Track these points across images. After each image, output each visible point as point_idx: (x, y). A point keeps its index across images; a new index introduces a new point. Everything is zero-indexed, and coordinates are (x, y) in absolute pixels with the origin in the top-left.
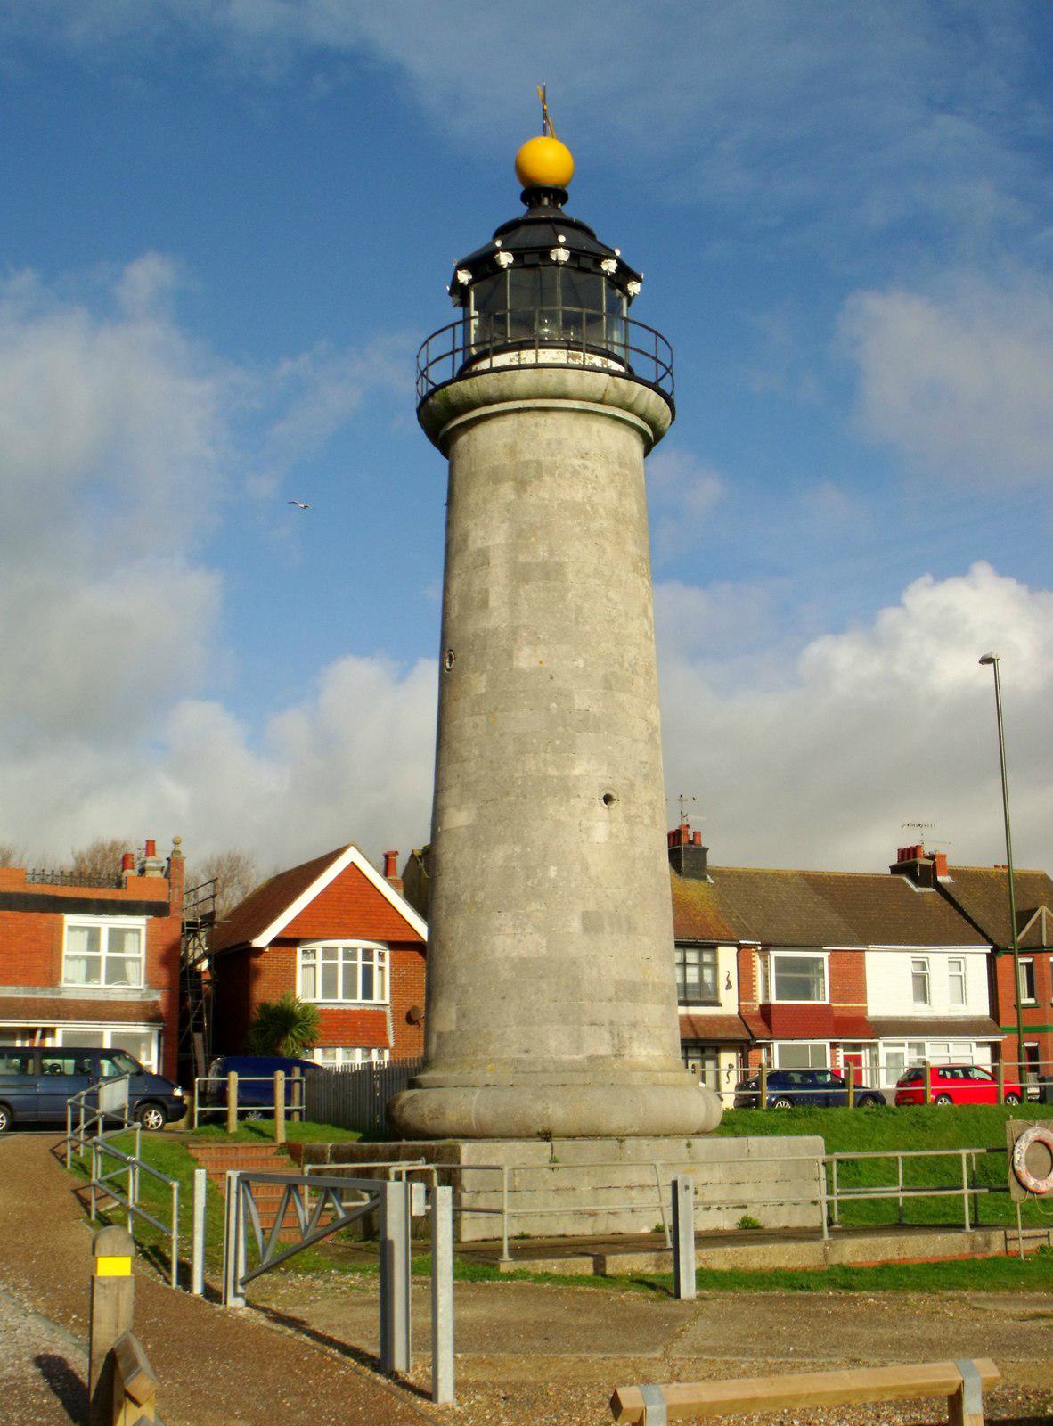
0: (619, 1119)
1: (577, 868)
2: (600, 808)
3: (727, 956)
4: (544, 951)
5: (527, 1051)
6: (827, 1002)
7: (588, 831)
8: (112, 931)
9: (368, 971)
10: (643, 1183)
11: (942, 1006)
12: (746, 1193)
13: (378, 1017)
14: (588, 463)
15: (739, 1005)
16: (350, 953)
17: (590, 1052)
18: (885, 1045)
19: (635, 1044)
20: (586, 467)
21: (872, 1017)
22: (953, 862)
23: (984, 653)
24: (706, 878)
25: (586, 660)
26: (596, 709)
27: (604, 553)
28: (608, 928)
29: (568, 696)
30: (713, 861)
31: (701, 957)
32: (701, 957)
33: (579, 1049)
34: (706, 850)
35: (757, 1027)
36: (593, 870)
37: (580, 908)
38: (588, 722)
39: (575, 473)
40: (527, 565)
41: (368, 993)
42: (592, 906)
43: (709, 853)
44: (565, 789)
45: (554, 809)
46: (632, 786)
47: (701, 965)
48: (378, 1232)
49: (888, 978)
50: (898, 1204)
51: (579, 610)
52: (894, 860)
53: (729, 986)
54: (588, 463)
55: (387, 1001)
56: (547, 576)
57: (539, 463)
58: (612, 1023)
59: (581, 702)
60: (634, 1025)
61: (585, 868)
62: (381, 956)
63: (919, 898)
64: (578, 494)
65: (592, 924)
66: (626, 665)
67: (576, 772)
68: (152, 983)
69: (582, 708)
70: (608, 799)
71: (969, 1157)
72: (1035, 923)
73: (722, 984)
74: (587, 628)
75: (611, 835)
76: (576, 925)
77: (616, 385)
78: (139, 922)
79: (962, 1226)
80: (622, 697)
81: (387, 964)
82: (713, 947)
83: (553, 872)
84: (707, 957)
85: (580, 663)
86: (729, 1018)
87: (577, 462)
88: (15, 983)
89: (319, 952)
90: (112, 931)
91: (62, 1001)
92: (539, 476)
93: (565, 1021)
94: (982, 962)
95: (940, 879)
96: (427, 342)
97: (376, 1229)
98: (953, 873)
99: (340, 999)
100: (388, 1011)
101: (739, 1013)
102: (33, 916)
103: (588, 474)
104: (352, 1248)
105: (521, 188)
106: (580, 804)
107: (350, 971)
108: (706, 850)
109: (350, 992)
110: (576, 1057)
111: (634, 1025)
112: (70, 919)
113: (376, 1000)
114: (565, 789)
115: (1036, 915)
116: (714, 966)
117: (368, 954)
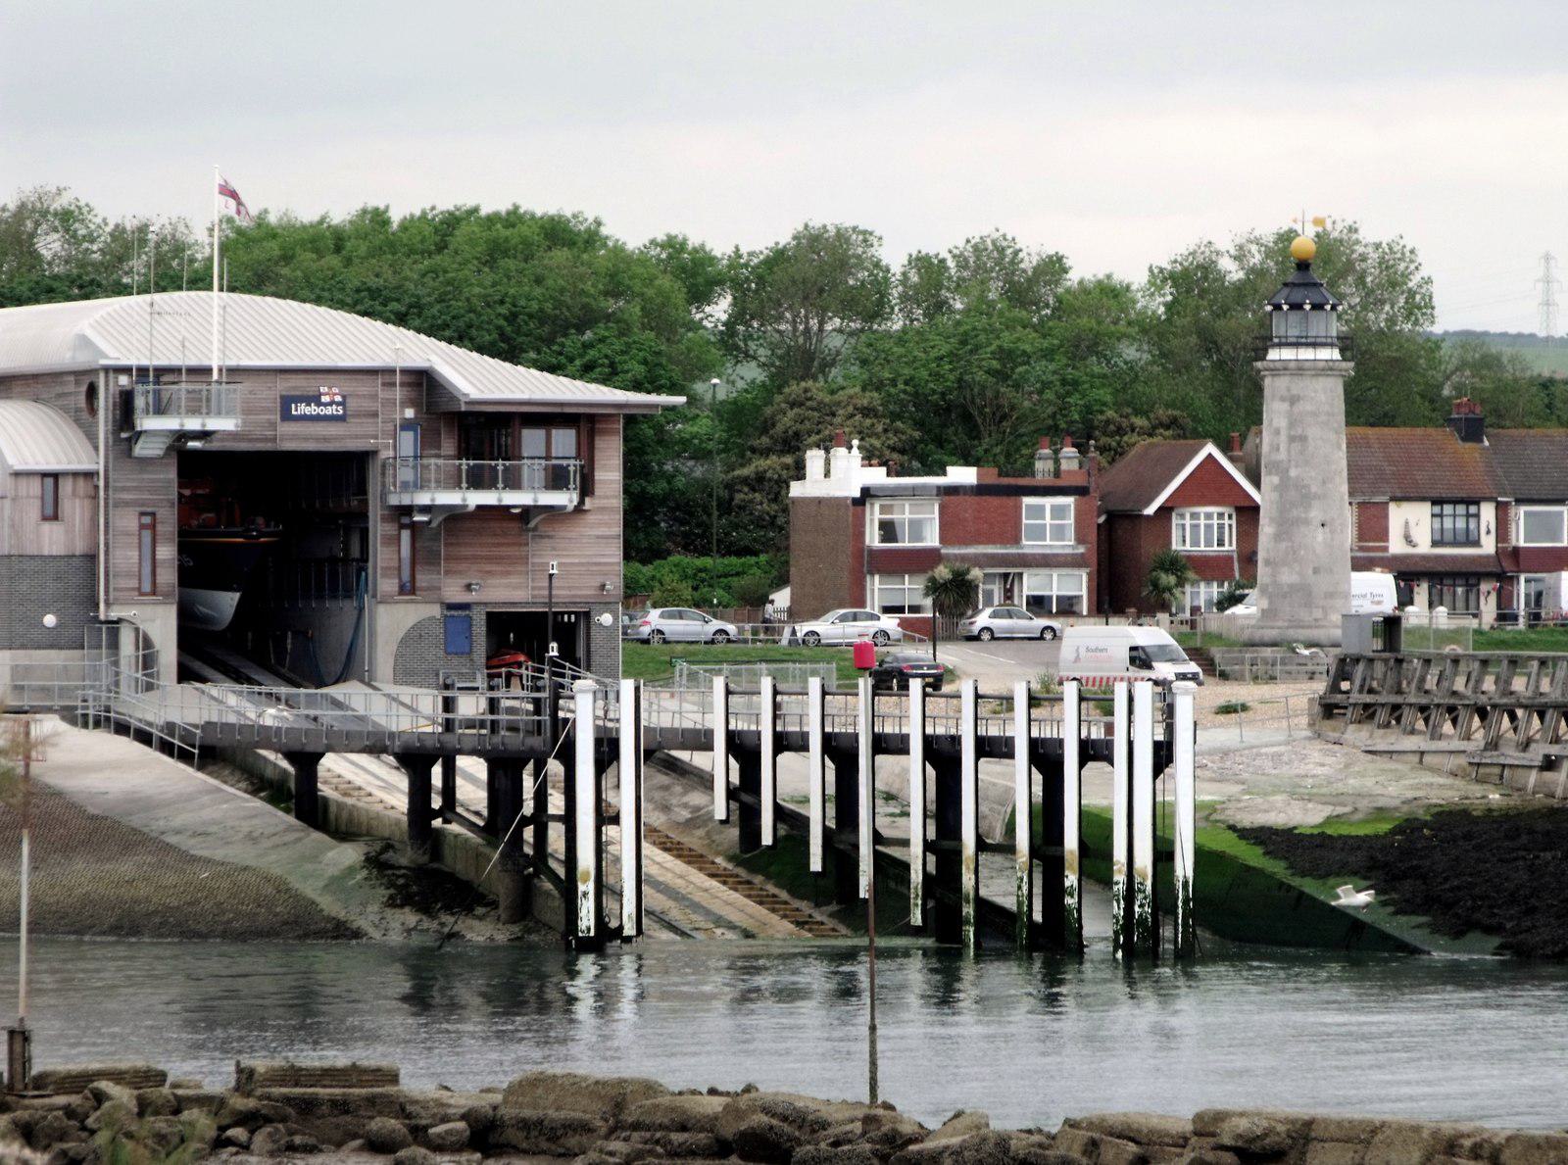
2: (1321, 529)
3: (1488, 512)
8: (1053, 508)
9: (1221, 527)
13: (1228, 559)
16: (1209, 516)
35: (1507, 565)
38: (1316, 497)
41: (1221, 543)
44: (1307, 522)
45: (1303, 529)
47: (1468, 516)
48: (1190, 976)
50: (293, 633)
53: (1488, 532)
55: (1234, 547)
59: (1314, 489)
62: (1230, 517)
64: (1309, 407)
65: (1316, 571)
68: (1080, 539)
76: (1310, 572)
81: (1234, 522)
82: (1477, 502)
84: (1473, 509)
86: (1488, 557)
89: (1188, 516)
90: (1053, 508)
97: (1197, 969)
99: (1202, 548)
100: (1235, 556)
104: (1010, 1022)
107: (1208, 527)
109: (1208, 543)
112: (1027, 501)
113: (1227, 548)
114: (1307, 522)
116: (1477, 516)
117: (1221, 516)
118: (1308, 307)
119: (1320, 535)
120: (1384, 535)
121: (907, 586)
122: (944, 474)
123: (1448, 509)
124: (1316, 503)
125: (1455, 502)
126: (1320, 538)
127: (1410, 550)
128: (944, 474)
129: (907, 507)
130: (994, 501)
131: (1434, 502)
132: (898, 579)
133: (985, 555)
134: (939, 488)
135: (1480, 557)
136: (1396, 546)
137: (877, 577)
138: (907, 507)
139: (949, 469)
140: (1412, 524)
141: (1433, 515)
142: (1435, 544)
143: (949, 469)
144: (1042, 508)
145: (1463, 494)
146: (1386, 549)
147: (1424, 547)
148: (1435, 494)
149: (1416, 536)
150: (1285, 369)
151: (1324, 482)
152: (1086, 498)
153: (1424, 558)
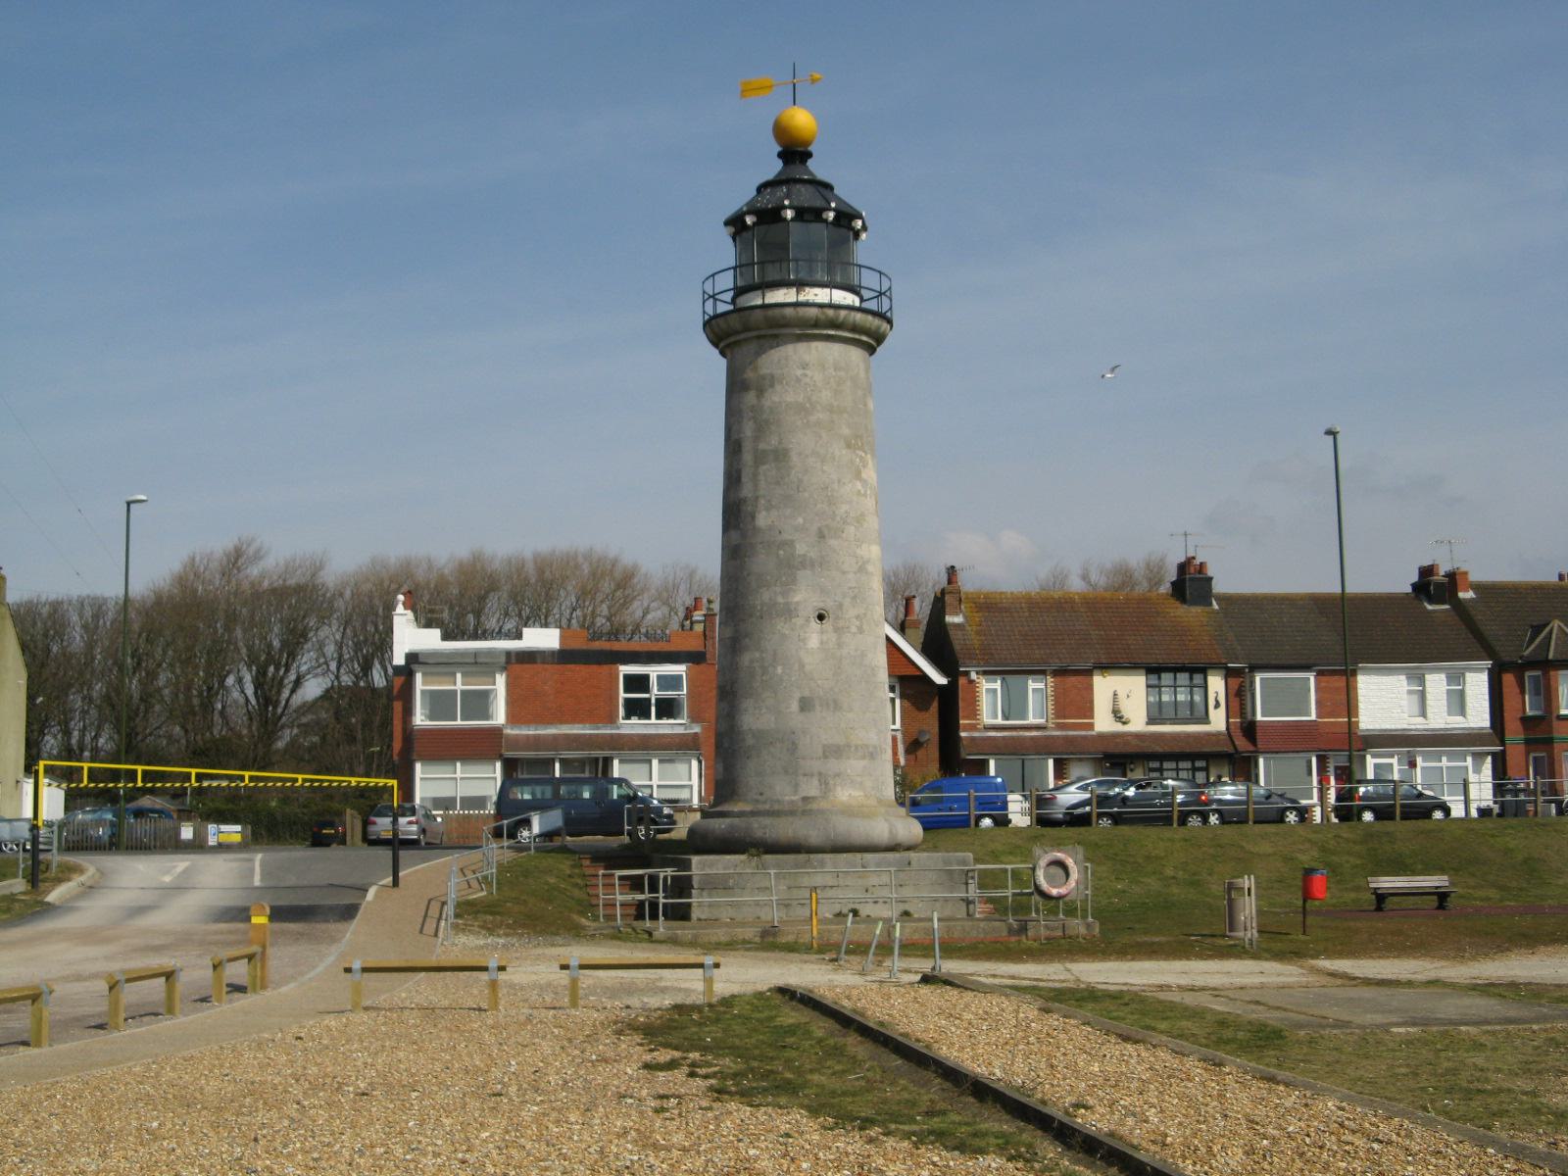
0: (814, 837)
1: (796, 667)
2: (815, 625)
3: (1216, 684)
4: (773, 726)
5: (761, 794)
6: (1313, 717)
7: (804, 641)
10: (825, 884)
11: (1440, 718)
12: (907, 892)
14: (808, 372)
15: (1227, 722)
17: (804, 794)
18: (1374, 756)
19: (839, 789)
20: (806, 375)
21: (1363, 731)
22: (1475, 576)
23: (1328, 426)
24: (1211, 604)
25: (804, 519)
26: (812, 555)
27: (821, 437)
28: (818, 708)
29: (791, 544)
30: (1220, 586)
31: (1191, 679)
32: (1191, 679)
33: (796, 792)
34: (1211, 579)
35: (1242, 743)
36: (808, 668)
37: (797, 695)
39: (798, 380)
40: (764, 451)
42: (807, 693)
43: (1214, 582)
45: (781, 626)
46: (840, 606)
49: (1383, 699)
51: (801, 481)
52: (1415, 578)
54: (808, 372)
56: (777, 459)
57: (772, 376)
58: (820, 774)
59: (801, 548)
60: (838, 775)
61: (802, 666)
63: (1430, 619)
65: (806, 705)
66: (838, 519)
67: (796, 599)
69: (802, 553)
70: (821, 617)
71: (665, 878)
72: (1545, 638)
73: (1211, 703)
74: (806, 495)
75: (822, 643)
76: (795, 706)
77: (823, 313)
78: (679, 669)
79: (621, 905)
80: (833, 542)
82: (1203, 671)
83: (779, 670)
84: (1198, 679)
85: (801, 520)
86: (1218, 734)
87: (799, 372)
88: (581, 721)
91: (620, 736)
92: (772, 386)
93: (786, 772)
94: (1484, 677)
95: (1461, 595)
96: (713, 275)
98: (1478, 587)
101: (1228, 729)
102: (594, 668)
103: (808, 380)
105: (779, 149)
106: (799, 621)
108: (1211, 579)
110: (793, 798)
111: (838, 775)
114: (789, 612)
115: (1547, 629)
118: (789, 214)
119: (814, 637)
120: (1088, 710)
121: (459, 775)
122: (519, 636)
123: (1167, 678)
124: (804, 576)
125: (1175, 670)
126: (814, 642)
127: (1119, 728)
128: (519, 636)
129: (459, 676)
130: (582, 671)
131: (1153, 670)
132: (451, 768)
133: (567, 737)
134: (508, 653)
135: (1209, 735)
136: (1103, 723)
137: (458, 764)
138: (459, 676)
139: (526, 631)
140: (1122, 695)
141: (1148, 686)
142: (1151, 721)
143: (526, 631)
144: (645, 678)
145: (1185, 660)
146: (1091, 726)
147: (1137, 722)
148: (1158, 657)
149: (1126, 713)
150: (747, 329)
151: (821, 536)
152: (703, 666)
153: (1138, 736)
